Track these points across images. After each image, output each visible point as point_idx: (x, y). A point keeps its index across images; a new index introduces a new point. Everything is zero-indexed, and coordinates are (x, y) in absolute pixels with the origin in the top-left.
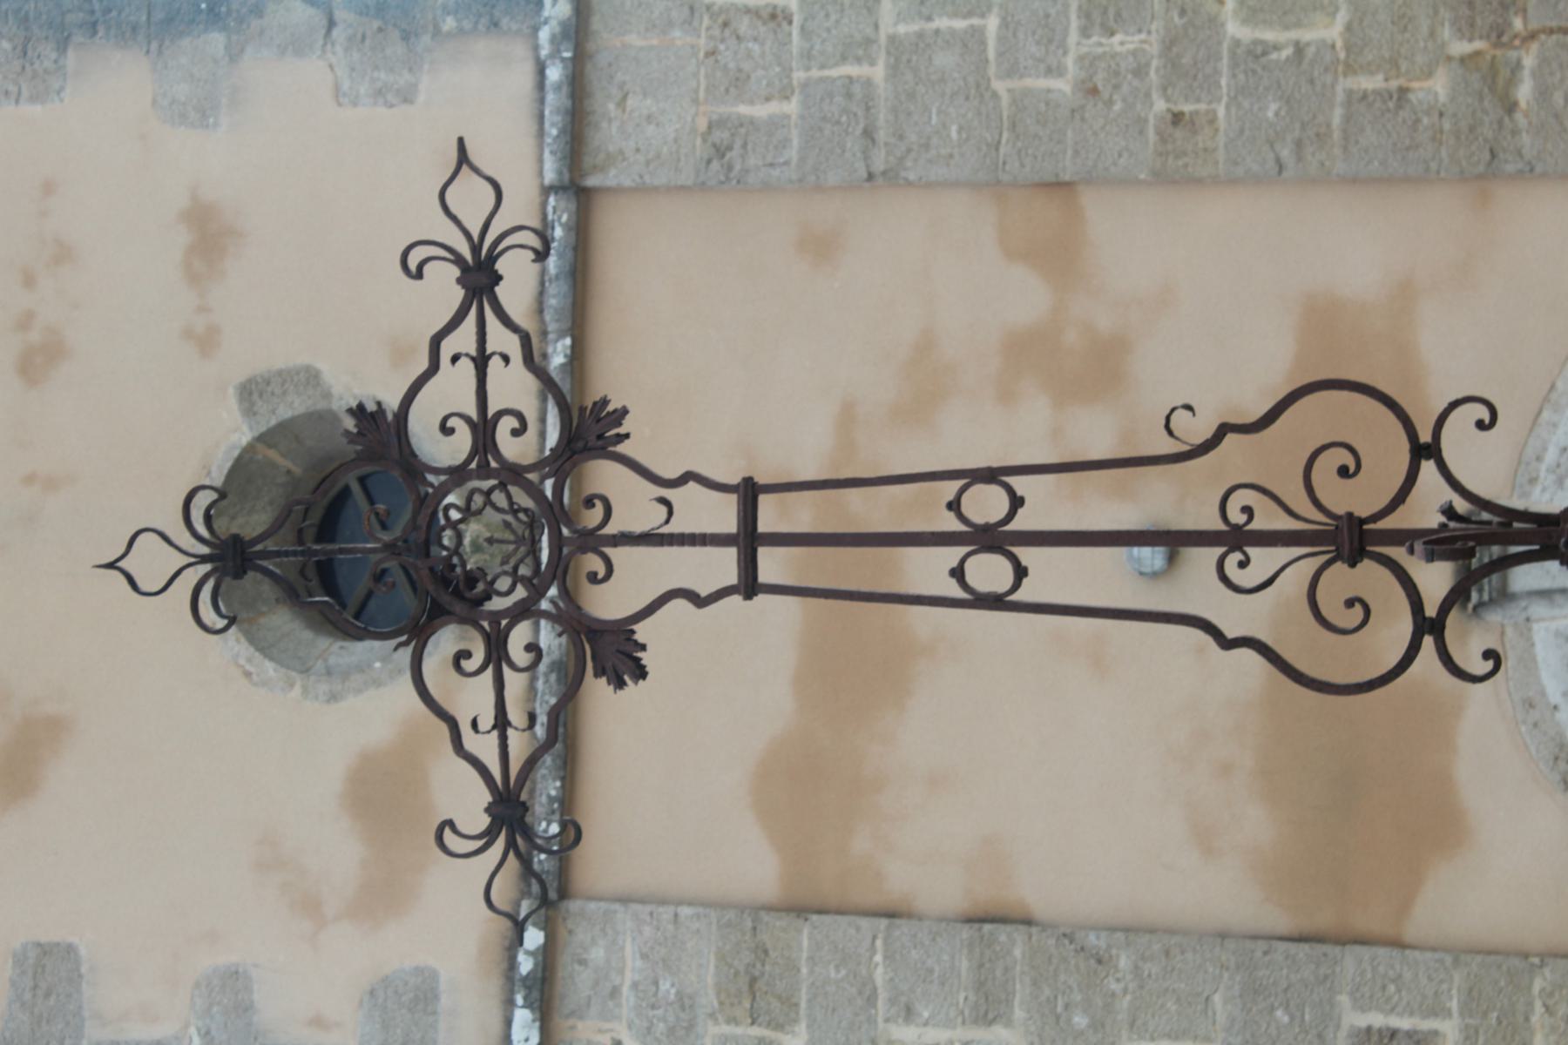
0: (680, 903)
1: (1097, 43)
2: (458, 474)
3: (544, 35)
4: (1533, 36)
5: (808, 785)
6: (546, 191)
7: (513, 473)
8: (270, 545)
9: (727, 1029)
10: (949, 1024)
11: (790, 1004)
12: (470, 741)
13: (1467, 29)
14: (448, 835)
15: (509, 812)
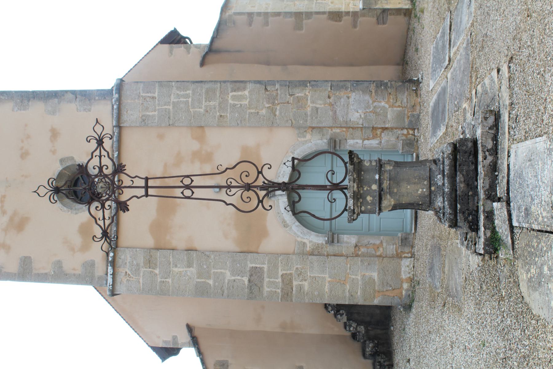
0: (137, 248)
1: (208, 103)
2: (96, 176)
3: (113, 100)
4: (279, 104)
5: (159, 228)
6: (114, 127)
7: (106, 176)
8: (63, 188)
9: (145, 269)
10: (183, 268)
11: (156, 265)
12: (99, 222)
13: (268, 102)
14: (95, 238)
15: (105, 234)
